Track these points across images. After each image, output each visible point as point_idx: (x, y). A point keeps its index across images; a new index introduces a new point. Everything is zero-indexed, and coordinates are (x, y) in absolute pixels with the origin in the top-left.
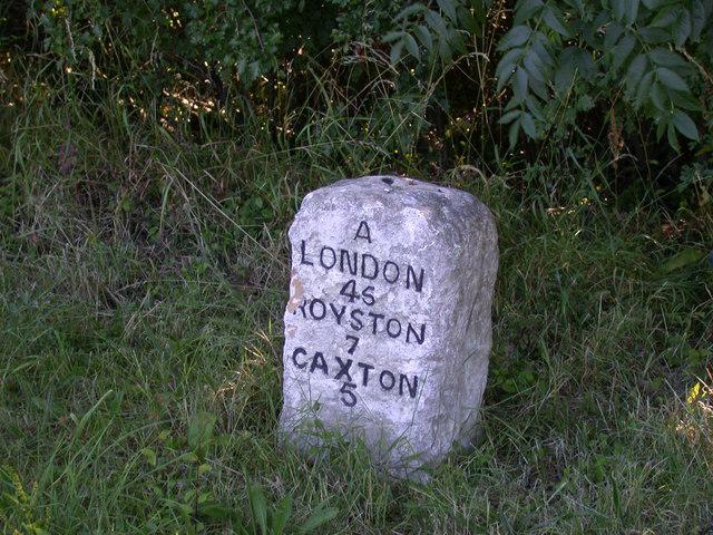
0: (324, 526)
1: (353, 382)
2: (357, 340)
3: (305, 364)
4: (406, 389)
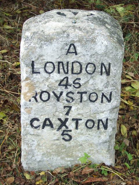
1: (69, 129)
2: (70, 107)
3: (39, 126)
4: (101, 126)
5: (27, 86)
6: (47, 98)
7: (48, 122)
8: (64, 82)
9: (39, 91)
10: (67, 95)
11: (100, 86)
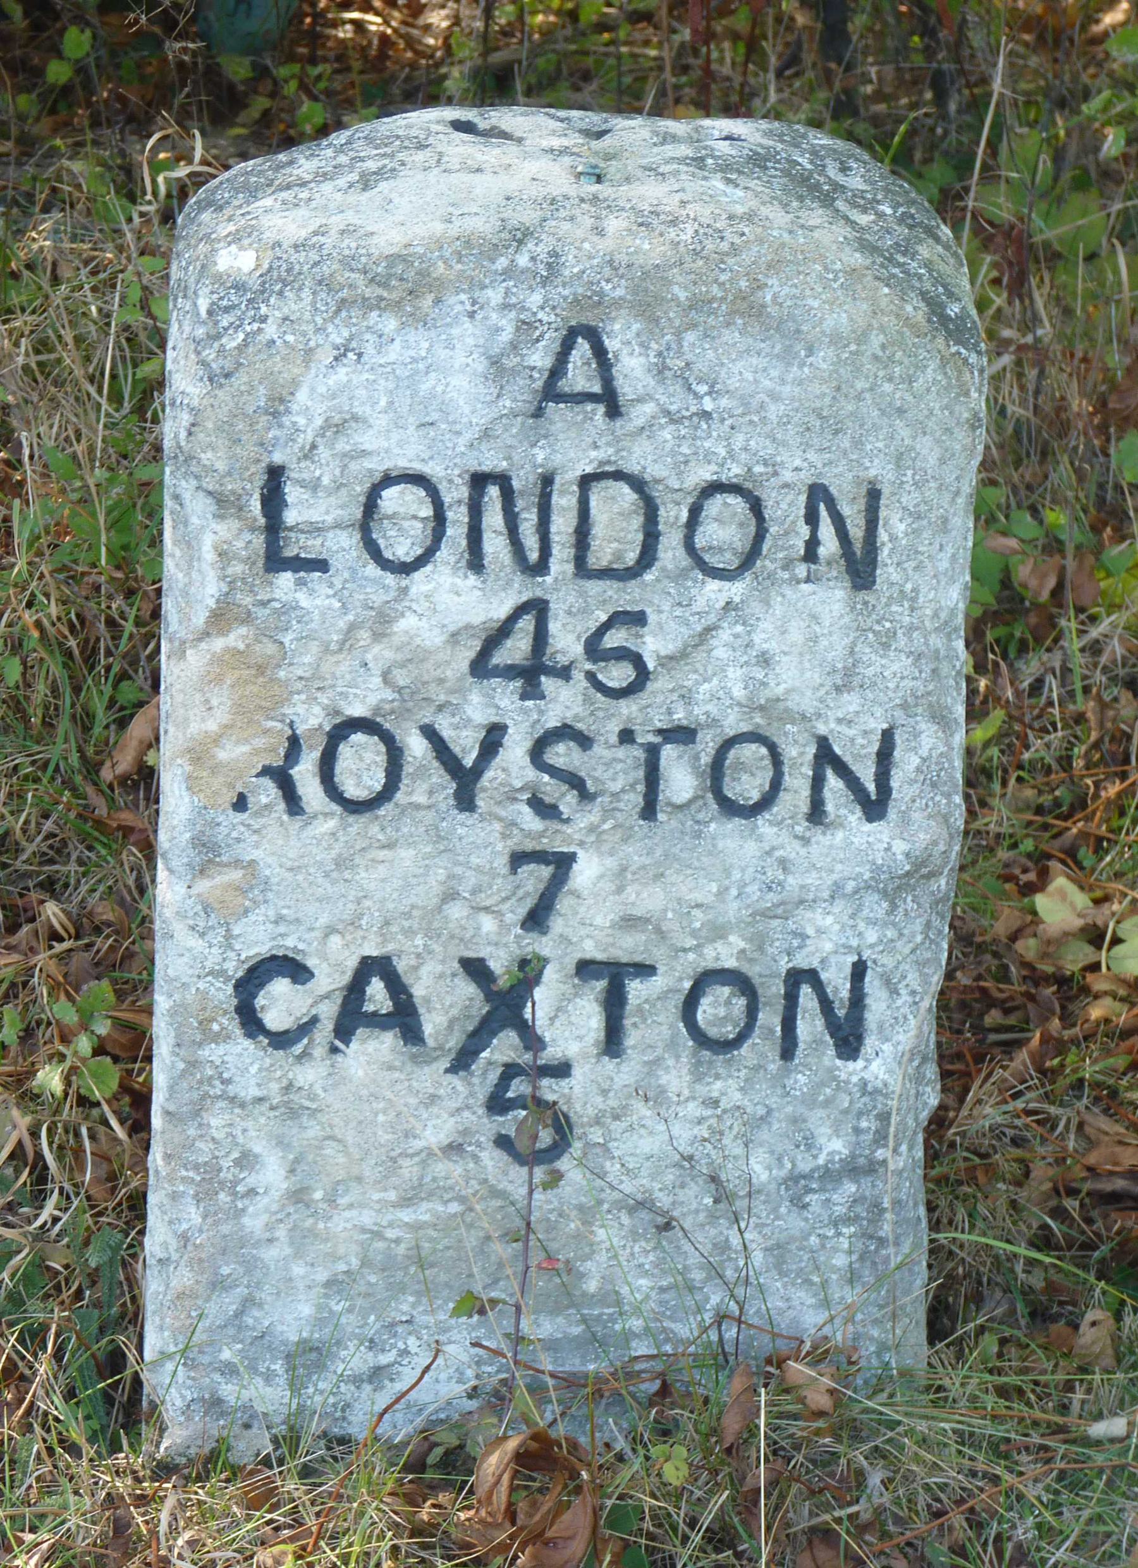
0: (41, 1207)
1: (551, 1054)
2: (563, 863)
3: (307, 1027)
4: (810, 1025)
5: (219, 680)
6: (376, 781)
7: (377, 994)
8: (516, 649)
9: (314, 722)
10: (537, 753)
11: (795, 680)
